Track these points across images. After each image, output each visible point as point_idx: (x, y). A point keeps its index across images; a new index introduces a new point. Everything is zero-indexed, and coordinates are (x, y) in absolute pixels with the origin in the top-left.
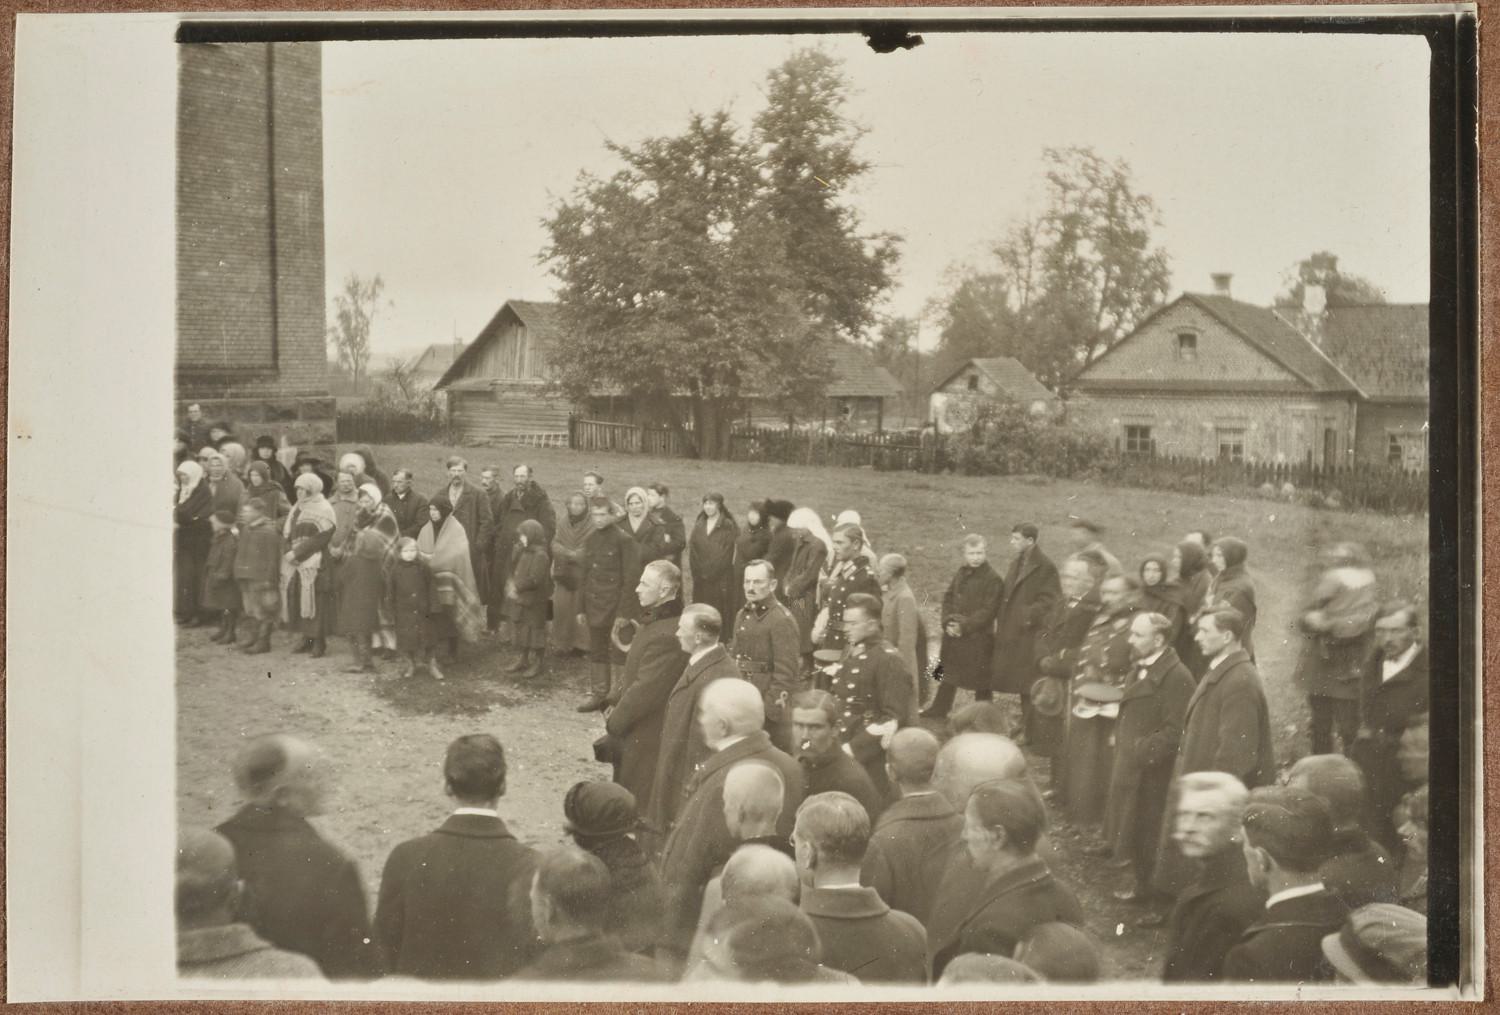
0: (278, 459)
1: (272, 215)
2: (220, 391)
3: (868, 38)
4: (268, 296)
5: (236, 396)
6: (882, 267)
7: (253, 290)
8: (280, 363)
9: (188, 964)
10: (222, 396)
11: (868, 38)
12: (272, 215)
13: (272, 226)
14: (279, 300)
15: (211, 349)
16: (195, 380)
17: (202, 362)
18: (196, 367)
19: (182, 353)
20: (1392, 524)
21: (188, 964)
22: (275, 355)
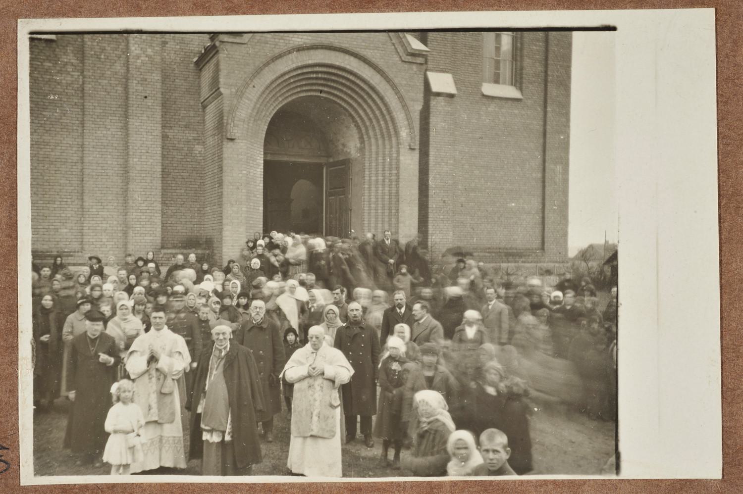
0: (396, 292)
1: (544, 177)
2: (517, 259)
3: (35, 407)
4: (541, 215)
5: (524, 262)
6: (220, 309)
7: (533, 212)
8: (545, 246)
9: (344, 475)
10: (518, 262)
11: (35, 407)
12: (544, 177)
13: (544, 182)
14: (546, 217)
15: (514, 240)
16: (37, 256)
17: (510, 246)
18: (507, 249)
19: (32, 249)
20: (229, 227)
21: (344, 475)
22: (543, 243)
